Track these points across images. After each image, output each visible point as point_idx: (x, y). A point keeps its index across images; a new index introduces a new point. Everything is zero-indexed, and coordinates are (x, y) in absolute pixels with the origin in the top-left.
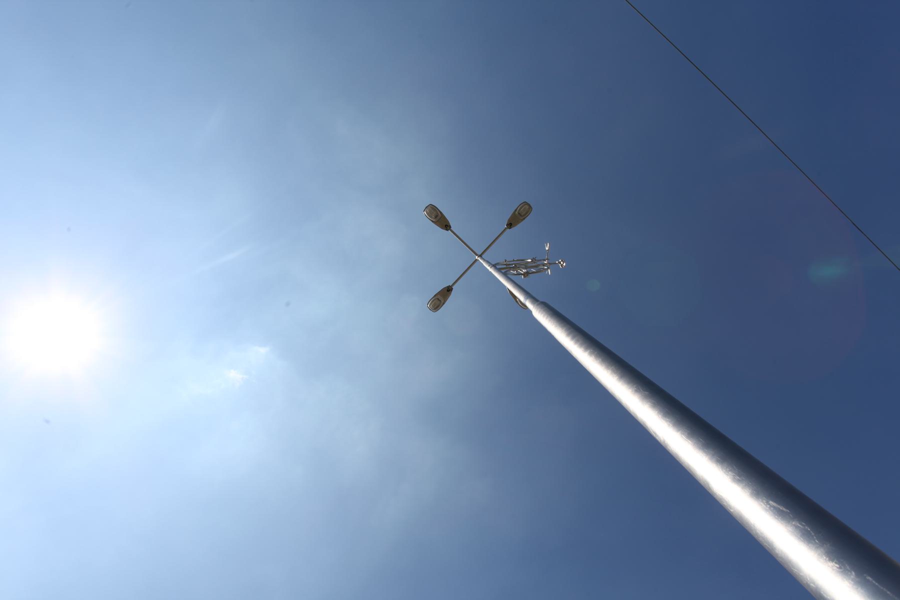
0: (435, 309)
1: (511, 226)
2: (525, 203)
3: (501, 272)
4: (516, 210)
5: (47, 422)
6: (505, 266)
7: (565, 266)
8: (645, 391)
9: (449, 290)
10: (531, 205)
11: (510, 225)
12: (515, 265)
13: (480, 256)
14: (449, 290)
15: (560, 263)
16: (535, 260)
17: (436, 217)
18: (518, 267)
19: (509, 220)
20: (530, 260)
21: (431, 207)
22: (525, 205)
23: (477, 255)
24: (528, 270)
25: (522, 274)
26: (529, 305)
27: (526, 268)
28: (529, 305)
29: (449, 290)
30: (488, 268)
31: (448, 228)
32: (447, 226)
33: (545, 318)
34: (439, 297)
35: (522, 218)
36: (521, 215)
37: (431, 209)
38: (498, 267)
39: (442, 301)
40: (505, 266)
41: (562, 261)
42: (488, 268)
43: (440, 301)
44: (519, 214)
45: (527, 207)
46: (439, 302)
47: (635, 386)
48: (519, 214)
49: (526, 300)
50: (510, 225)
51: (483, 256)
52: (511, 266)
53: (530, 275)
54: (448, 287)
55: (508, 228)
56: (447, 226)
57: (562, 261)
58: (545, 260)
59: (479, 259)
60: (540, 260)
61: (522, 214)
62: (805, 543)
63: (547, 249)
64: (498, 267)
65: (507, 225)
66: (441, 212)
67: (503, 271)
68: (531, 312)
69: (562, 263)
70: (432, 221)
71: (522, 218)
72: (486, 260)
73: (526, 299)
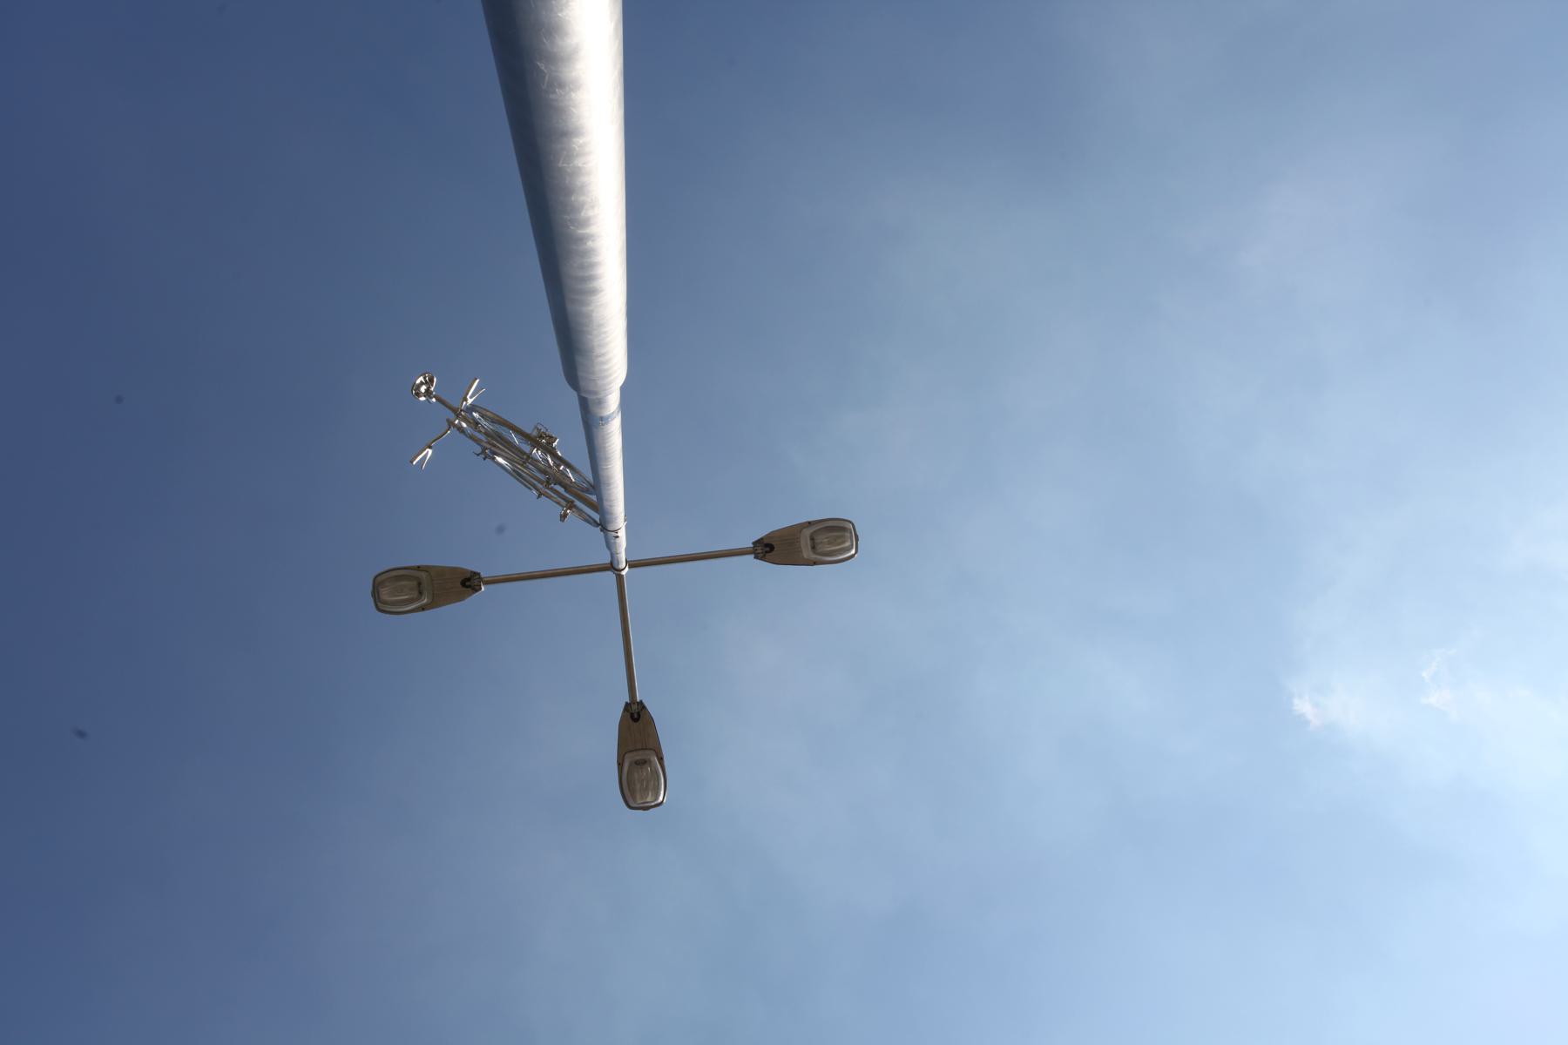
0: (844, 529)
1: (469, 579)
2: (380, 605)
3: (600, 499)
4: (423, 608)
5: (501, 530)
6: (578, 503)
7: (423, 374)
8: (542, 71)
9: (766, 545)
10: (371, 589)
11: (469, 583)
12: (548, 483)
13: (612, 567)
14: (768, 549)
15: (427, 390)
16: (484, 449)
17: (643, 763)
18: (544, 472)
19: (460, 598)
20: (500, 460)
21: (634, 799)
22: (385, 603)
23: (620, 579)
24: (526, 448)
25: (554, 455)
26: (613, 401)
27: (529, 456)
28: (613, 401)
29: (768, 549)
30: (622, 534)
31: (635, 707)
32: (636, 716)
33: (600, 271)
34: (807, 553)
35: (423, 575)
36: (419, 584)
37: (638, 796)
38: (597, 517)
39: (807, 532)
40: (578, 503)
41: (418, 394)
42: (622, 534)
43: (812, 539)
44: (421, 593)
45: (385, 594)
46: (819, 539)
47: (552, 96)
48: (421, 593)
49: (609, 417)
50: (469, 583)
51: (608, 561)
52: (561, 490)
53: (528, 431)
54: (476, 574)
55: (480, 579)
56: (636, 716)
57: (418, 394)
58: (460, 429)
59: (623, 565)
60: (472, 438)
61: (415, 583)
62: (577, 171)
63: (430, 452)
64: (597, 517)
65: (476, 589)
66: (620, 765)
67: (594, 498)
68: (624, 389)
69: (423, 389)
70: (661, 759)
71: (423, 575)
72: (608, 553)
73: (604, 420)
